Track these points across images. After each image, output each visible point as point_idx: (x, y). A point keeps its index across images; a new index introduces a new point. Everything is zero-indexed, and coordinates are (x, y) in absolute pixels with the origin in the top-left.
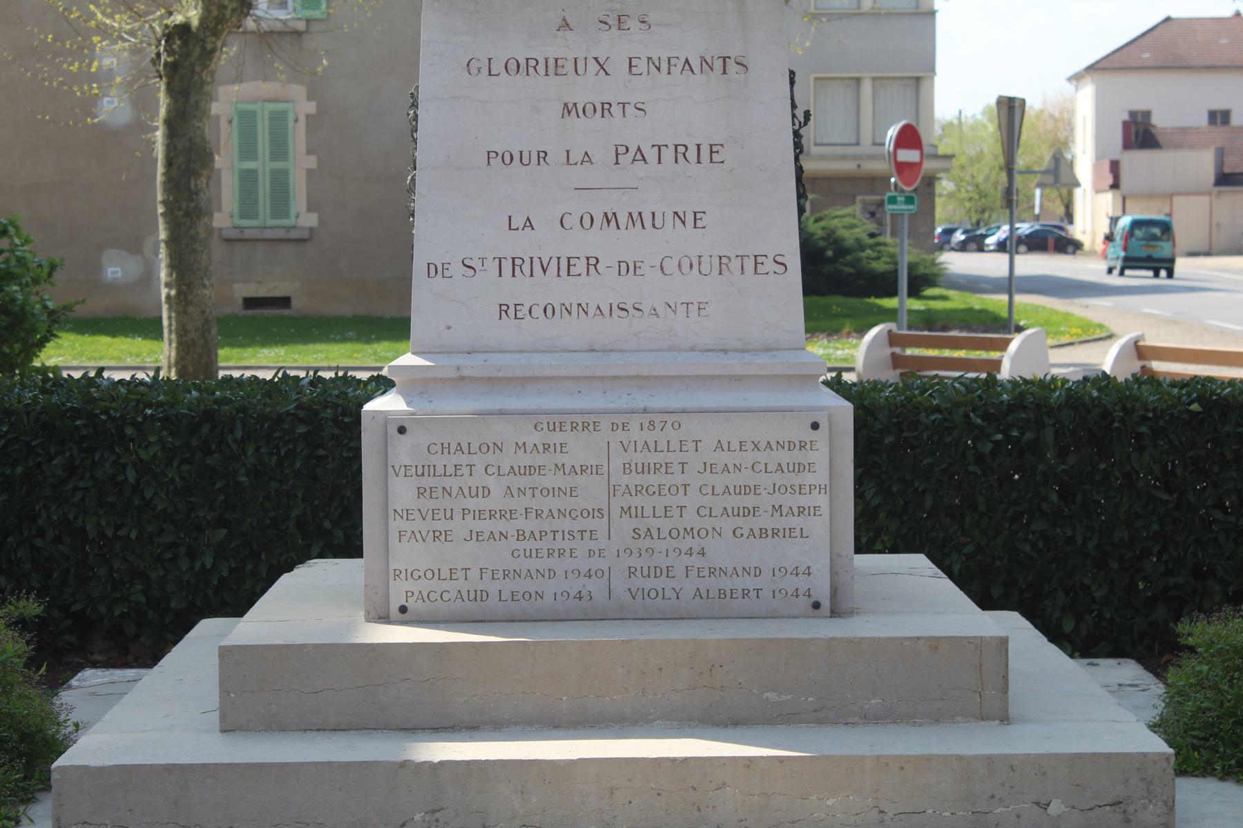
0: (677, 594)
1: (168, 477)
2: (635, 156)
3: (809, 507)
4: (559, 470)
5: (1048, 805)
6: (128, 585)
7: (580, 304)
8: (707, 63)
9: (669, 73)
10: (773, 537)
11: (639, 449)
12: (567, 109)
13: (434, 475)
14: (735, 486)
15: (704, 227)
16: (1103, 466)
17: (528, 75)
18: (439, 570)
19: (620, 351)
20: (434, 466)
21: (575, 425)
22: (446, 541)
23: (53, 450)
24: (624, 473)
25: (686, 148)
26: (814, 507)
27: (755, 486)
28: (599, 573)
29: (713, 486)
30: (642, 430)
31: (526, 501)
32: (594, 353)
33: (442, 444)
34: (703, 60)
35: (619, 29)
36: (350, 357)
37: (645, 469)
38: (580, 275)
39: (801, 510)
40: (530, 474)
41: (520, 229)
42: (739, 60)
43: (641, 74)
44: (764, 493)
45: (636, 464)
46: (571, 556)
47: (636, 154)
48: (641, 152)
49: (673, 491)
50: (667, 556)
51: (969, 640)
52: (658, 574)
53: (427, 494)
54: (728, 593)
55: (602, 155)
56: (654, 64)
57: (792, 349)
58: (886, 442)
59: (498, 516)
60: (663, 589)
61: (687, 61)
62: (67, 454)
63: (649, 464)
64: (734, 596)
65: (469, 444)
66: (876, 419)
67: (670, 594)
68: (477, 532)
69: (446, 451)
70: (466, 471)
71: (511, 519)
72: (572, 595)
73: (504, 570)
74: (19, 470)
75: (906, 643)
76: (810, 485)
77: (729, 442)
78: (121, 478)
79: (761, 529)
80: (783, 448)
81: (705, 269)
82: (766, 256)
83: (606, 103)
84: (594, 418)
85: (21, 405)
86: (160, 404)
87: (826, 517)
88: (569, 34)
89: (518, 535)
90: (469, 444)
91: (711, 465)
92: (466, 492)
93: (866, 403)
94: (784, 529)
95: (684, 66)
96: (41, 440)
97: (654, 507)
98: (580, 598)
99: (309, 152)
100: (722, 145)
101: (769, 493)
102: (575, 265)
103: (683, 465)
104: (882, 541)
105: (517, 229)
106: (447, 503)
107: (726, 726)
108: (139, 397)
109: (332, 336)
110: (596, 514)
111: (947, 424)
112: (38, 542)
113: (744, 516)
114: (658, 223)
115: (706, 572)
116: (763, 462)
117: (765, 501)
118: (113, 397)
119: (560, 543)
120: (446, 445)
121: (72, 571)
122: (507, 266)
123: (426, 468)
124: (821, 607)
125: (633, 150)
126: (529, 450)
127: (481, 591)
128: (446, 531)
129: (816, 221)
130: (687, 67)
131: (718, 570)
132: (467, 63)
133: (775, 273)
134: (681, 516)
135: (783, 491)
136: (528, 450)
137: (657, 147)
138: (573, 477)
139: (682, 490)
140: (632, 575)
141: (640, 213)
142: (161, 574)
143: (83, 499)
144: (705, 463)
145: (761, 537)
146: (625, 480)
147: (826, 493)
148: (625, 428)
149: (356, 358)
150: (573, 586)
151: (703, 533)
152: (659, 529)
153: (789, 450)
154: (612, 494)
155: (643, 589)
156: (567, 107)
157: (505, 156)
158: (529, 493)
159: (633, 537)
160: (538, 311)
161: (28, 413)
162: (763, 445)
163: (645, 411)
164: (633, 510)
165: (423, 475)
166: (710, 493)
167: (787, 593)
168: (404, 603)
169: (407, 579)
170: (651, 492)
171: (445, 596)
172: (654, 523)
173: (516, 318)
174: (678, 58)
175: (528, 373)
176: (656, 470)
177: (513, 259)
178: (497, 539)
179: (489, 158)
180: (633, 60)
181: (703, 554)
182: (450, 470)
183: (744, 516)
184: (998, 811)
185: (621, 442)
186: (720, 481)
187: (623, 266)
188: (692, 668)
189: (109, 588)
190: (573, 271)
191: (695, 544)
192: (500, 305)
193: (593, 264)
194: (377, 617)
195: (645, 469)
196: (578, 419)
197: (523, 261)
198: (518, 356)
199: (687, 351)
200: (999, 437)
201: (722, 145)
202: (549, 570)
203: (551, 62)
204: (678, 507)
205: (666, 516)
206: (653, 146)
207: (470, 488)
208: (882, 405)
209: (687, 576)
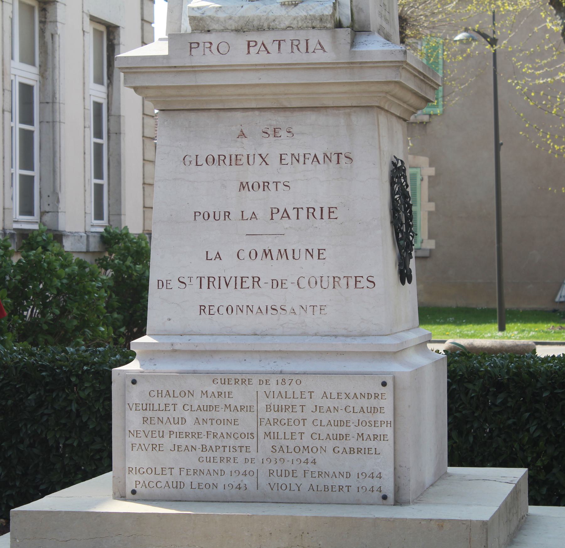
0: (299, 488)
1: (96, 408)
2: (283, 214)
3: (380, 435)
4: (227, 408)
6: (73, 474)
7: (248, 306)
8: (328, 157)
9: (304, 163)
10: (358, 453)
11: (276, 397)
12: (243, 186)
13: (153, 410)
14: (334, 421)
15: (324, 259)
17: (219, 165)
18: (155, 468)
19: (273, 335)
20: (153, 404)
21: (237, 381)
22: (159, 450)
23: (29, 391)
24: (267, 411)
25: (314, 209)
26: (384, 435)
27: (347, 421)
28: (251, 473)
29: (321, 421)
30: (277, 384)
31: (207, 427)
32: (256, 336)
33: (158, 391)
34: (325, 155)
35: (275, 136)
37: (279, 409)
38: (248, 288)
39: (376, 436)
40: (210, 411)
41: (213, 259)
42: (347, 155)
43: (287, 164)
44: (352, 426)
45: (274, 405)
46: (234, 462)
47: (284, 213)
48: (286, 212)
49: (297, 423)
50: (293, 463)
52: (287, 475)
53: (149, 421)
54: (330, 488)
55: (263, 214)
56: (295, 158)
57: (378, 335)
58: (544, 395)
59: (190, 436)
60: (290, 484)
61: (315, 156)
62: (37, 393)
63: (282, 405)
64: (334, 490)
65: (174, 391)
66: (537, 381)
67: (294, 487)
68: (178, 446)
69: (160, 395)
70: (171, 408)
71: (198, 438)
72: (234, 487)
73: (194, 470)
74: (10, 402)
75: (422, 523)
76: (381, 421)
77: (331, 393)
78: (68, 409)
79: (350, 448)
80: (364, 397)
81: (325, 285)
82: (362, 277)
83: (266, 182)
84: (248, 376)
85: (12, 363)
86: (94, 364)
87: (391, 442)
88: (244, 140)
89: (203, 448)
90: (174, 391)
91: (320, 407)
92: (172, 420)
93: (531, 370)
94: (365, 448)
95: (314, 159)
96: (22, 384)
97: (285, 433)
98: (240, 488)
99: (430, 200)
100: (336, 208)
101: (355, 426)
102: (245, 282)
103: (302, 407)
104: (542, 460)
105: (211, 259)
106: (161, 427)
108: (82, 359)
109: (438, 320)
110: (250, 436)
112: (21, 447)
113: (340, 439)
114: (297, 256)
116: (352, 406)
117: (353, 430)
118: (67, 359)
119: (227, 454)
120: (160, 392)
121: (41, 465)
122: (205, 282)
123: (148, 405)
124: (388, 498)
125: (282, 211)
126: (209, 395)
127: (180, 482)
128: (159, 445)
130: (315, 159)
131: (324, 473)
132: (183, 158)
133: (368, 287)
134: (301, 439)
135: (364, 424)
136: (209, 396)
137: (296, 209)
138: (236, 413)
139: (302, 422)
140: (271, 475)
141: (285, 250)
142: (93, 468)
143: (47, 421)
144: (316, 406)
145: (350, 453)
146: (267, 415)
147: (391, 426)
148: (267, 383)
149: (448, 335)
150: (235, 481)
151: (315, 450)
152: (288, 446)
153: (368, 399)
154: (259, 424)
155: (278, 484)
156: (243, 184)
157: (205, 215)
158: (209, 422)
159: (272, 451)
160: (223, 310)
161: (16, 368)
162: (352, 395)
163: (281, 373)
164: (272, 434)
165: (146, 409)
166: (319, 425)
167: (366, 489)
168: (134, 488)
169: (136, 474)
170: (283, 423)
171: (159, 485)
172: (285, 443)
173: (209, 314)
174: (310, 154)
175: (214, 348)
176: (286, 410)
177: (209, 278)
178: (190, 450)
179: (195, 216)
180: (282, 155)
181: (315, 463)
182: (163, 407)
183: (340, 439)
185: (265, 392)
186: (325, 417)
187: (275, 282)
188: (290, 534)
189: (62, 476)
190: (245, 285)
191: (310, 456)
192: (201, 306)
193: (256, 281)
194: (120, 497)
195: (279, 409)
196: (239, 377)
197: (215, 279)
198: (210, 337)
199: (313, 336)
201: (336, 208)
202: (221, 470)
203: (233, 157)
204: (299, 433)
205: (292, 439)
206: (294, 208)
207: (174, 418)
208: (542, 371)
209: (305, 477)
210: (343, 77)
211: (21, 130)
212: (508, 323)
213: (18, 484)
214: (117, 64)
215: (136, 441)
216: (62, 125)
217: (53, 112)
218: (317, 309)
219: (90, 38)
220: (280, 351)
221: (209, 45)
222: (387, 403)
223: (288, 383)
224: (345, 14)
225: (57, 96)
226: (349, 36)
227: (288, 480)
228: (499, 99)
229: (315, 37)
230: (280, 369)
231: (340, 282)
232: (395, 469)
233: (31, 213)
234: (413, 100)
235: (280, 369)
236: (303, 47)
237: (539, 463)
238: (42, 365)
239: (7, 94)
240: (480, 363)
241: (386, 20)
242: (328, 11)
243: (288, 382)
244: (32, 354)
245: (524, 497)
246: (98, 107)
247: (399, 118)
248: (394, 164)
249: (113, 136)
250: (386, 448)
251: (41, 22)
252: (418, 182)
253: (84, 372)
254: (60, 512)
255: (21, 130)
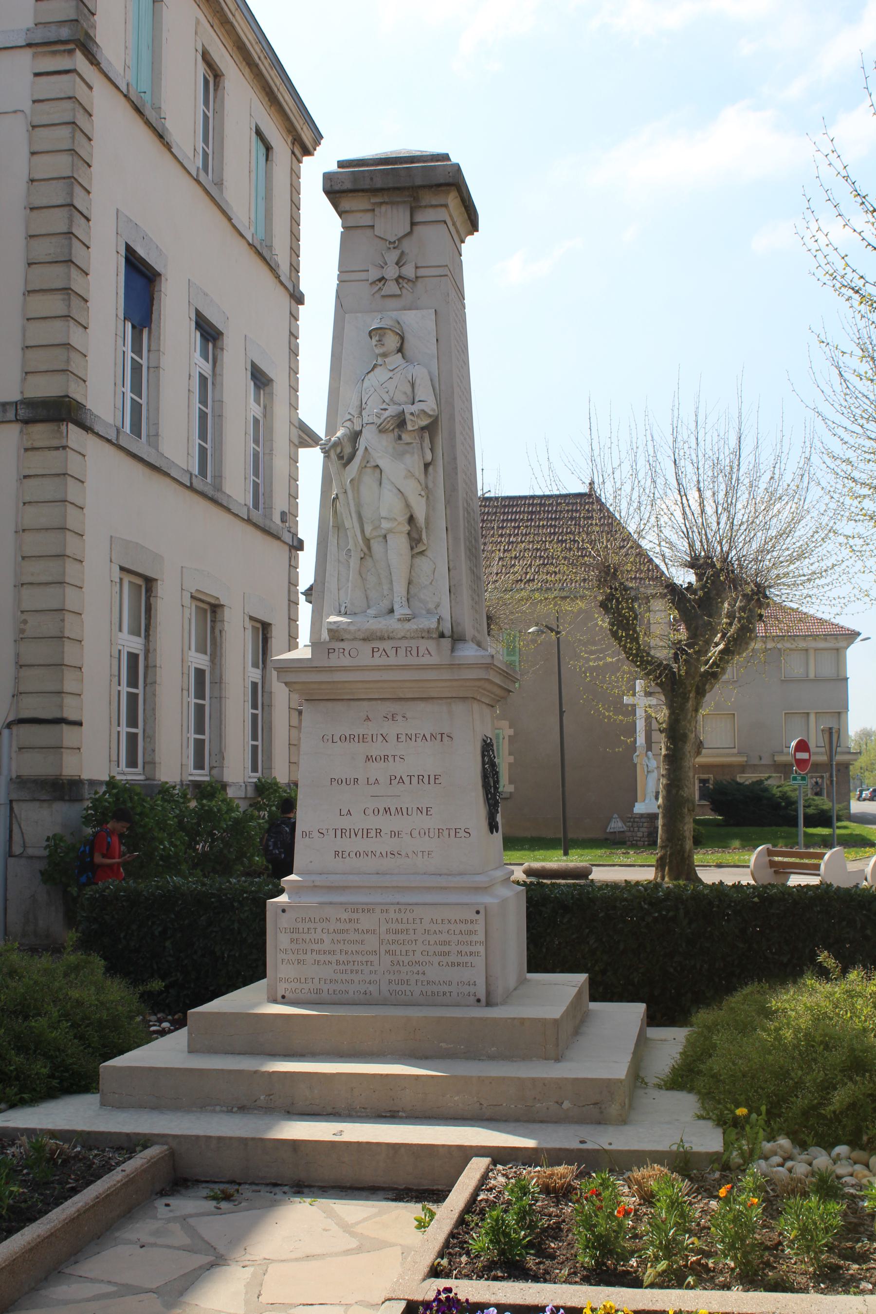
5: (562, 1103)
12: (368, 758)
16: (709, 929)
34: (432, 735)
36: (522, 858)
37: (397, 932)
51: (539, 1020)
54: (436, 994)
61: (424, 735)
67: (408, 993)
74: (186, 922)
81: (432, 835)
86: (252, 892)
88: (369, 723)
92: (438, 942)
99: (510, 754)
107: (422, 1059)
111: (630, 907)
114: (410, 813)
115: (425, 983)
119: (356, 967)
122: (339, 833)
125: (398, 778)
129: (778, 787)
135: (462, 943)
139: (414, 942)
151: (424, 964)
158: (342, 942)
160: (353, 855)
162: (453, 921)
163: (398, 904)
164: (391, 952)
168: (284, 994)
172: (401, 958)
184: (538, 1105)
187: (393, 833)
191: (420, 969)
193: (379, 832)
195: (397, 932)
200: (656, 915)
203: (361, 736)
210: (446, 675)
211: (196, 704)
212: (573, 849)
213: (192, 986)
214: (269, 665)
215: (284, 956)
216: (227, 700)
217: (221, 689)
218: (426, 854)
219: (249, 633)
220: (397, 887)
221: (342, 651)
222: (480, 927)
223: (403, 912)
224: (447, 628)
225: (224, 677)
226: (450, 644)
227: (404, 987)
228: (562, 676)
229: (424, 644)
230: (397, 901)
231: (444, 833)
232: (486, 978)
233: (202, 768)
234: (498, 691)
235: (397, 901)
236: (414, 652)
237: (597, 968)
238: (211, 893)
239: (185, 676)
240: (550, 891)
241: (477, 630)
242: (434, 625)
243: (403, 911)
244: (204, 884)
245: (586, 996)
246: (254, 685)
247: (488, 705)
248: (484, 741)
249: (266, 708)
250: (480, 962)
251: (212, 621)
252: (501, 740)
253: (244, 898)
254: (225, 1013)
255: (196, 704)
